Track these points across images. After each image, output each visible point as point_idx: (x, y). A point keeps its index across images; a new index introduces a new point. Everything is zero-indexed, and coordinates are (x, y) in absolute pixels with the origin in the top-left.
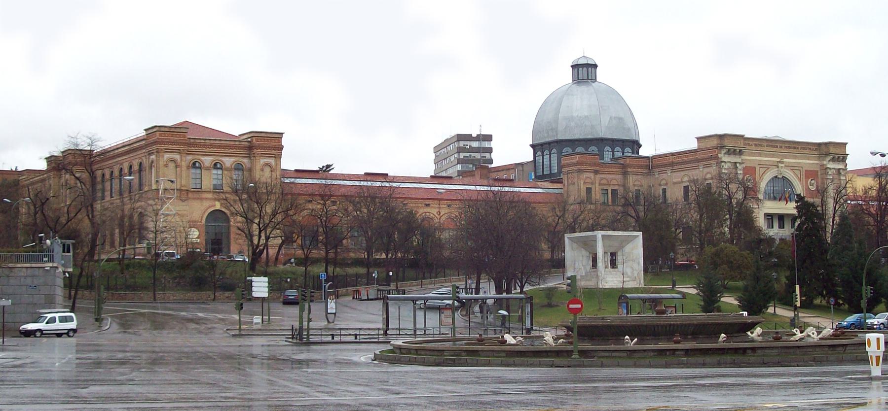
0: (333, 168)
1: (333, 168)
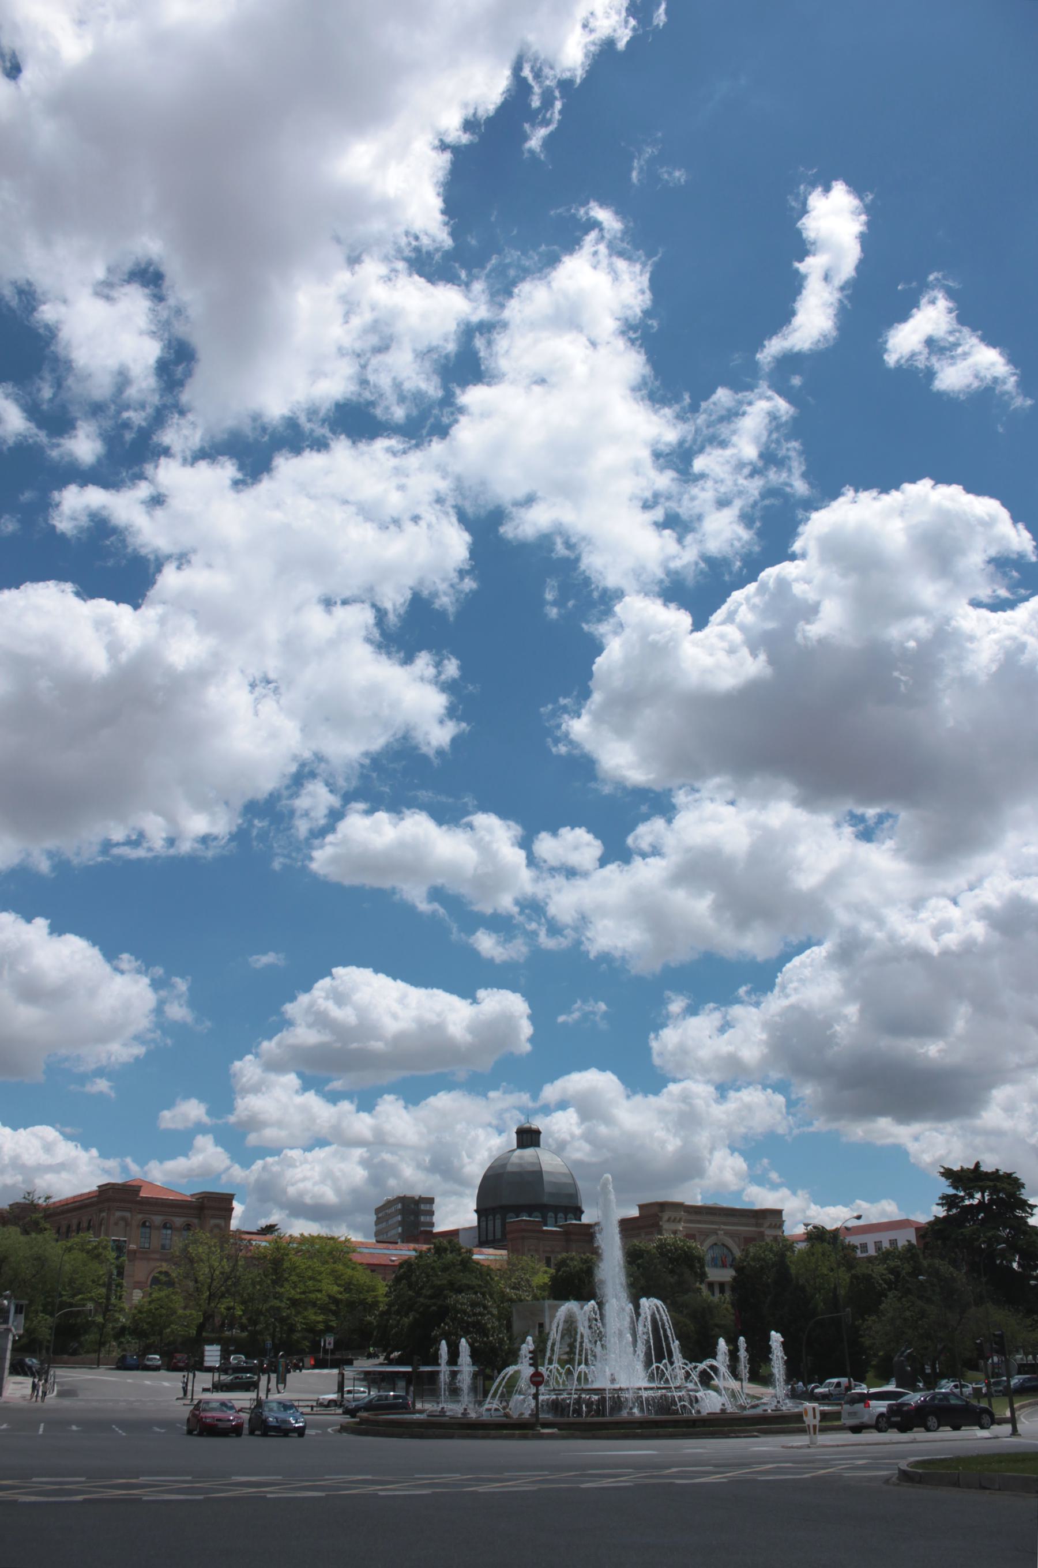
0: (783, 1447)
1: (783, 1447)
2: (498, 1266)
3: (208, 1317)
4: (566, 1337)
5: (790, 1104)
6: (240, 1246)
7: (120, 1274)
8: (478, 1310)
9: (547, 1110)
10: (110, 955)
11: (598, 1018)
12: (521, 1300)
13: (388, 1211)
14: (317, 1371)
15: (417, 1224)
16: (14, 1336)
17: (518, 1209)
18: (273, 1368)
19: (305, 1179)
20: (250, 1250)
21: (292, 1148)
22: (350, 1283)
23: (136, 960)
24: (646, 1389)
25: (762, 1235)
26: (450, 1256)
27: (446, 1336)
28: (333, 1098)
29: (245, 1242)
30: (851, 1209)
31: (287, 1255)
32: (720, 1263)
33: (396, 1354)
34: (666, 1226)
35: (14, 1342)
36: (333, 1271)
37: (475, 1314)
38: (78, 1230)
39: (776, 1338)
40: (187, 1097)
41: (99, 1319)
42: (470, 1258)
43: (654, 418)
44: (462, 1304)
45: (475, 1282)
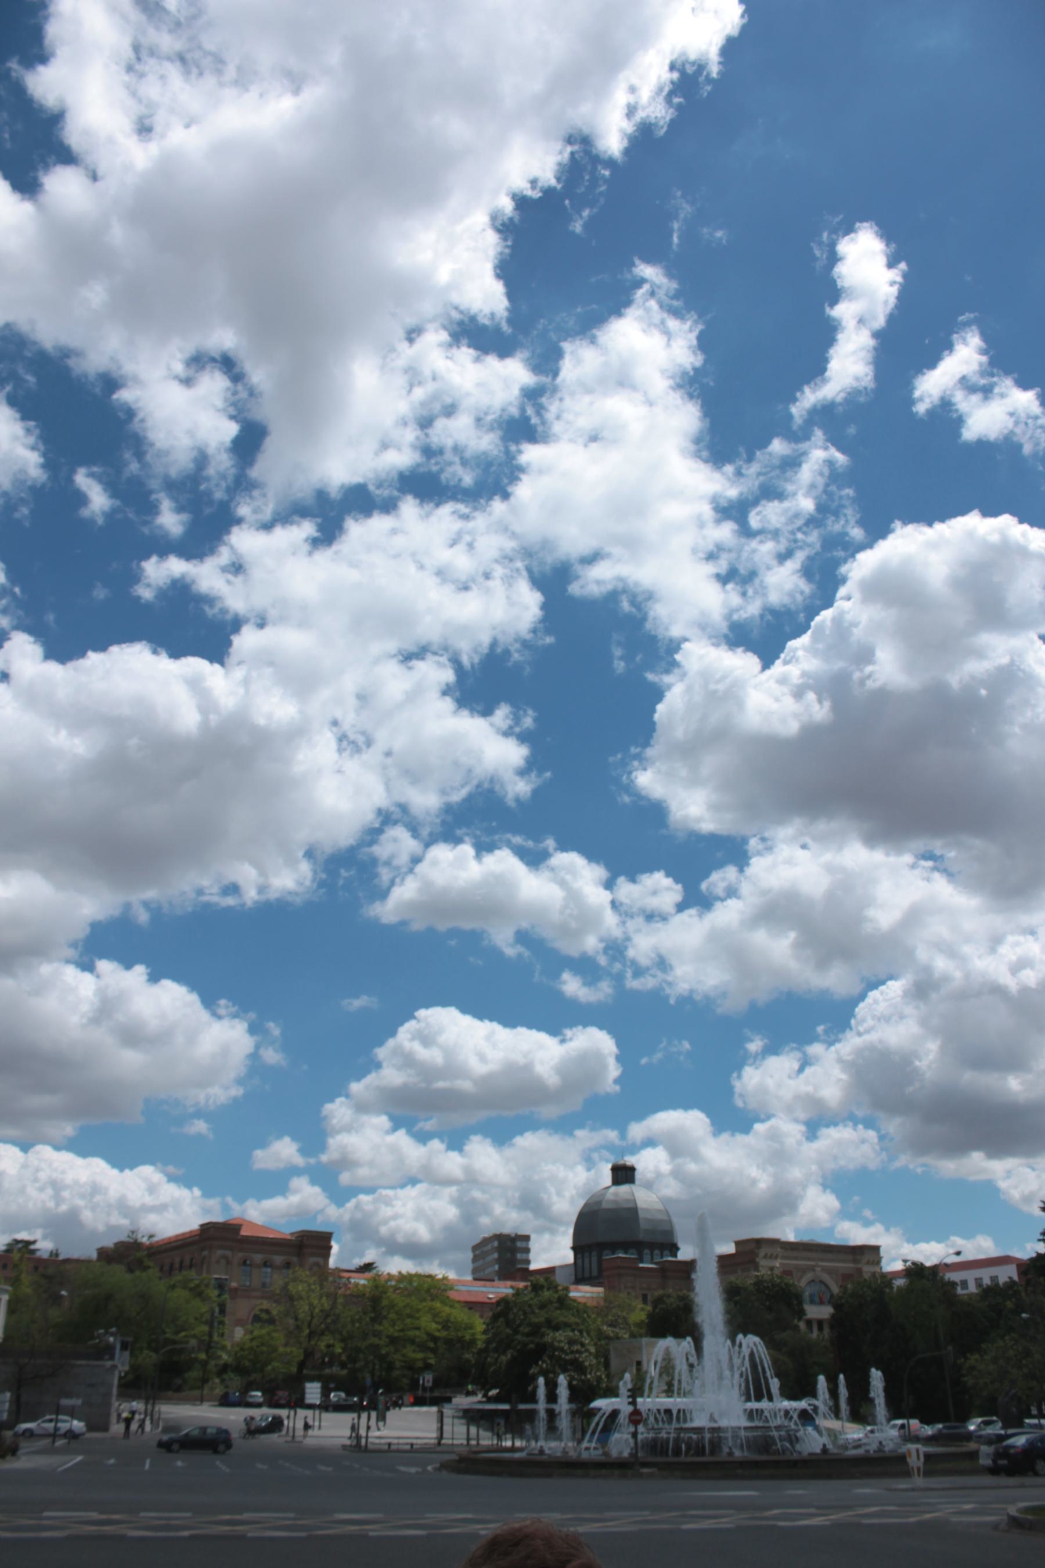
2: (595, 1304)
3: (308, 1354)
4: (664, 1376)
5: (882, 1138)
6: (339, 1284)
7: (222, 1311)
8: (575, 1348)
9: (634, 1149)
10: (209, 1002)
11: (682, 1058)
12: (618, 1338)
13: (485, 1249)
14: (416, 1409)
15: (513, 1261)
16: (120, 1372)
17: (614, 1246)
18: (373, 1406)
19: (395, 1217)
20: (349, 1288)
21: (385, 1188)
22: (448, 1321)
23: (234, 1005)
24: (746, 1428)
25: (859, 1271)
26: (546, 1294)
27: (545, 1373)
28: (422, 1138)
29: (344, 1280)
30: (947, 1246)
31: (386, 1293)
32: (817, 1299)
33: (493, 1392)
34: (763, 1262)
35: (120, 1378)
36: (431, 1309)
37: (572, 1352)
38: (181, 1268)
39: (876, 1376)
40: (280, 1137)
41: (203, 1356)
42: (567, 1296)
43: (717, 475)
44: (560, 1341)
45: (573, 1320)
